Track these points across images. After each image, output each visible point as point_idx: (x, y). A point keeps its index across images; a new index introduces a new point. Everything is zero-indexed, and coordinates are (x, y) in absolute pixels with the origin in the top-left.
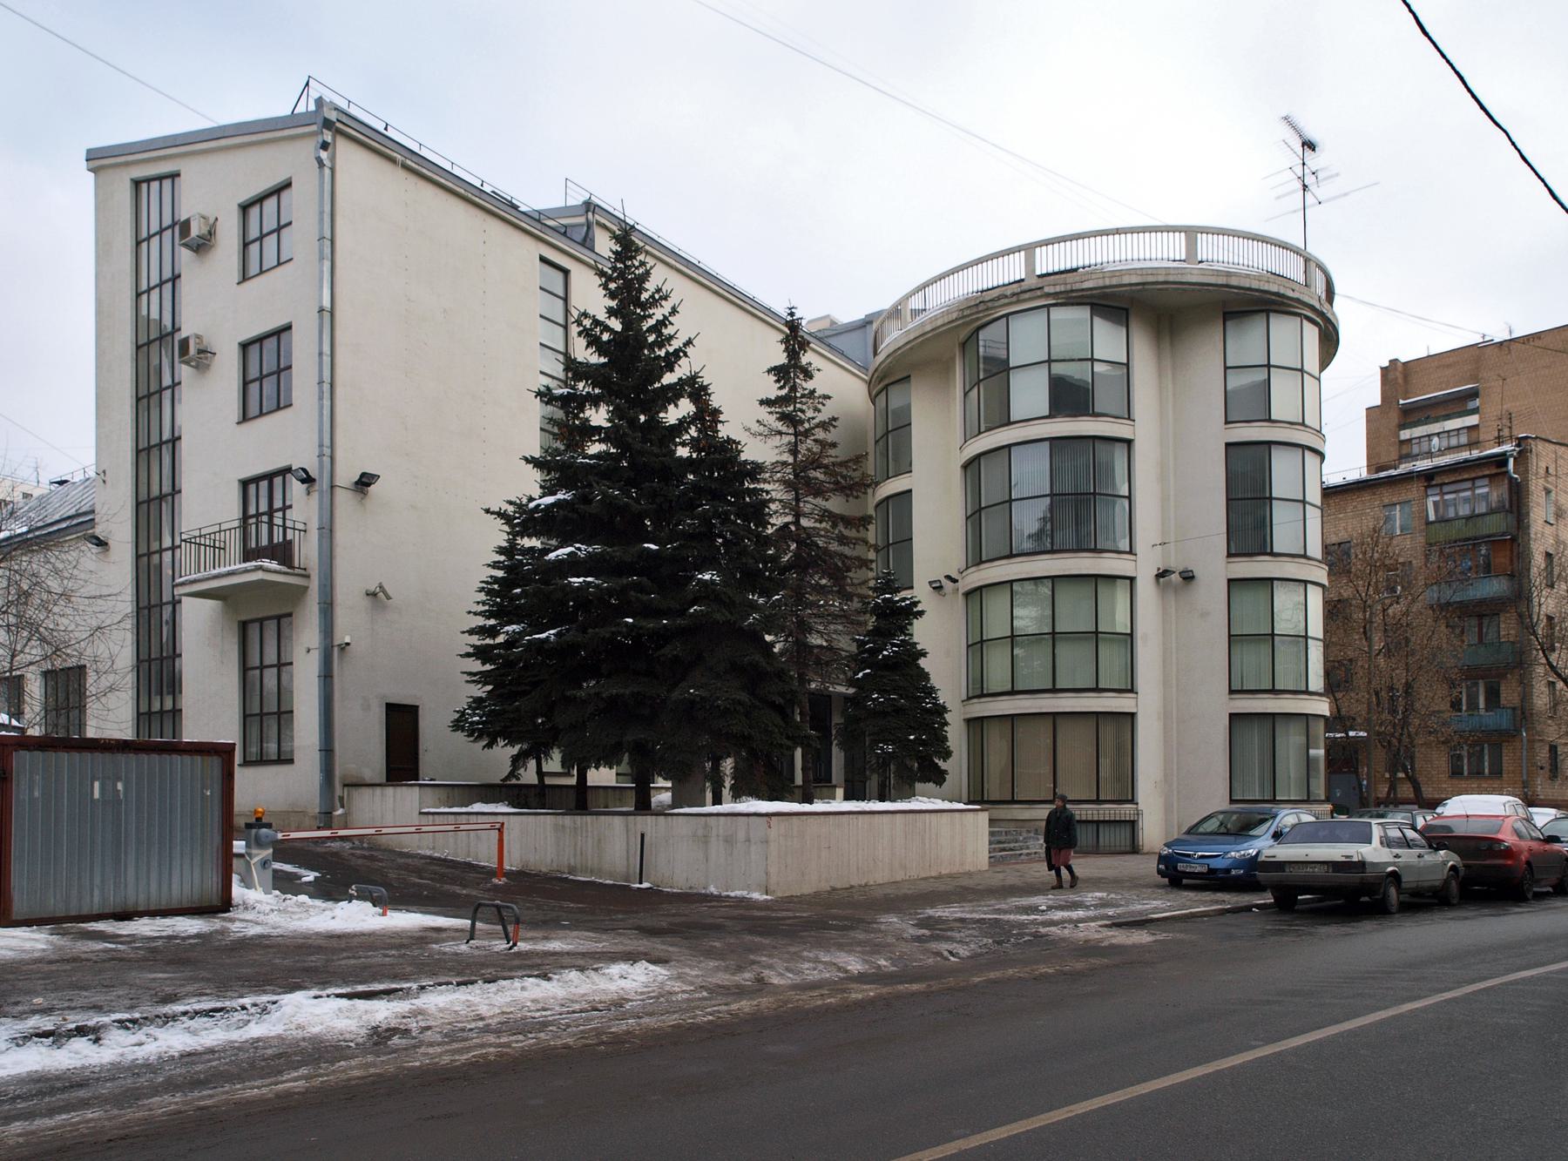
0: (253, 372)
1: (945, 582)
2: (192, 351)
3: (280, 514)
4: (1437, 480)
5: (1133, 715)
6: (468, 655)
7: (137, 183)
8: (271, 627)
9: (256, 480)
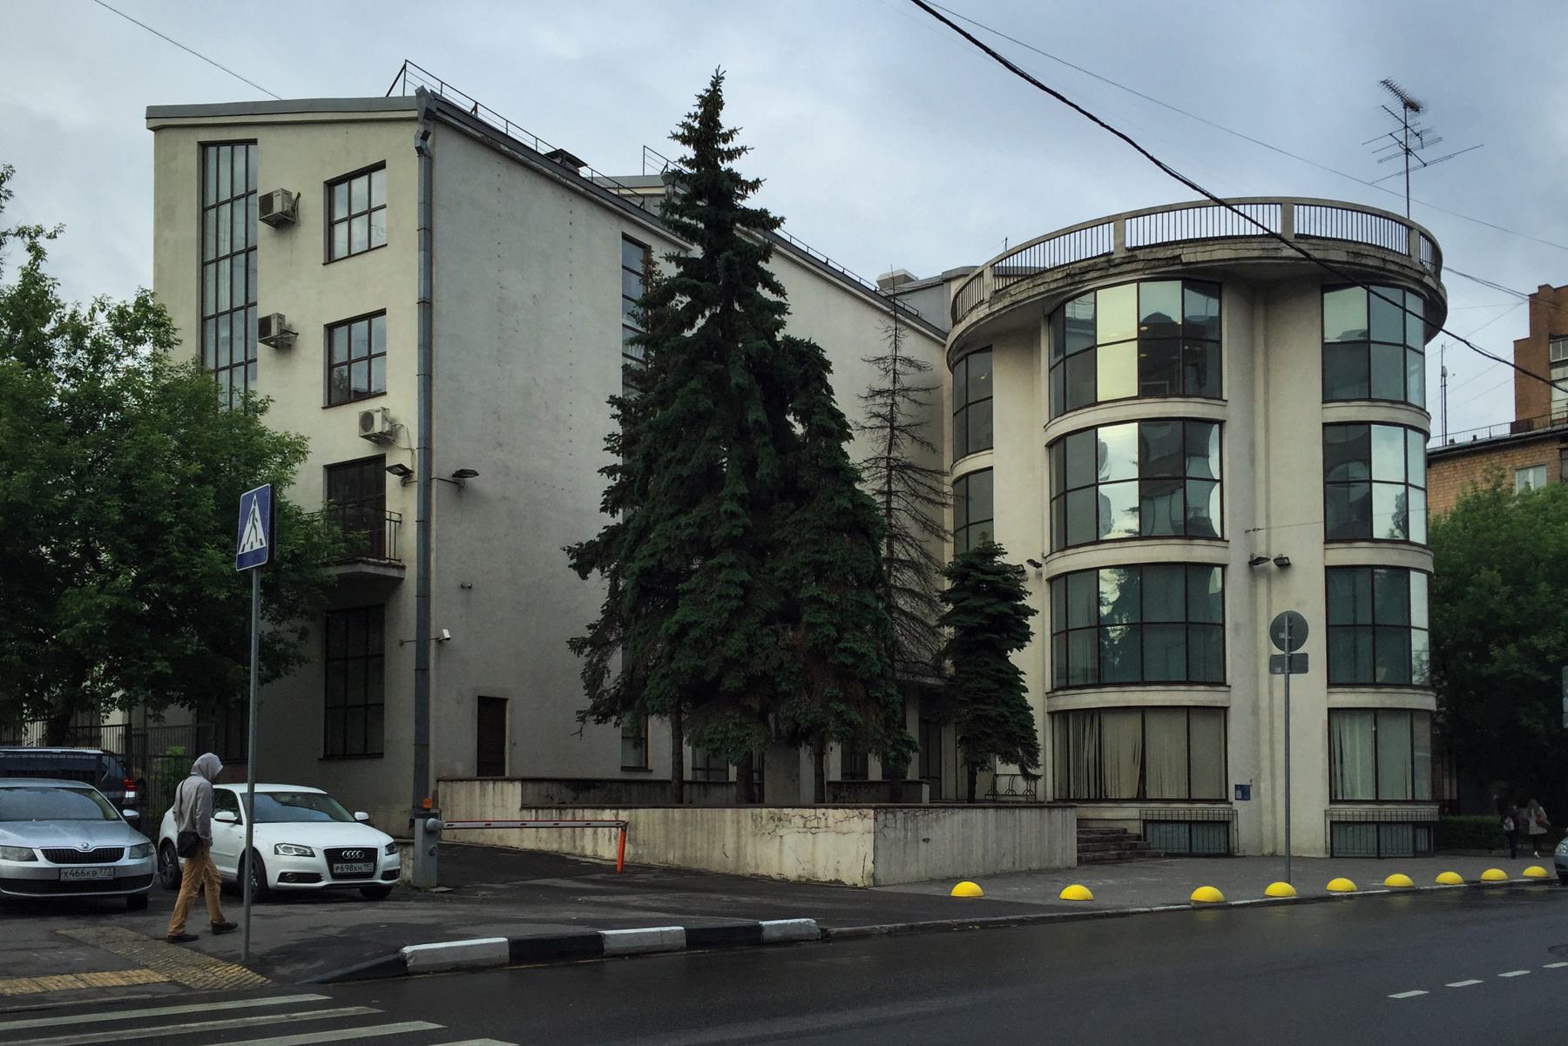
2: (274, 331)
5: (1225, 709)
7: (204, 146)
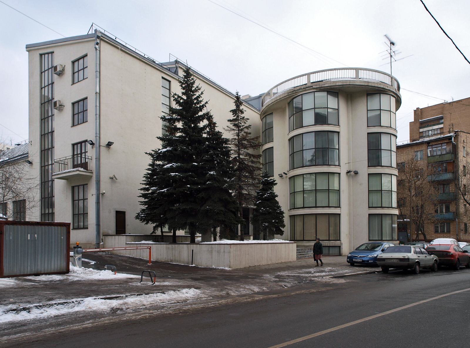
1: (284, 175)
2: (58, 105)
5: (339, 214)
7: (41, 55)
8: (81, 188)
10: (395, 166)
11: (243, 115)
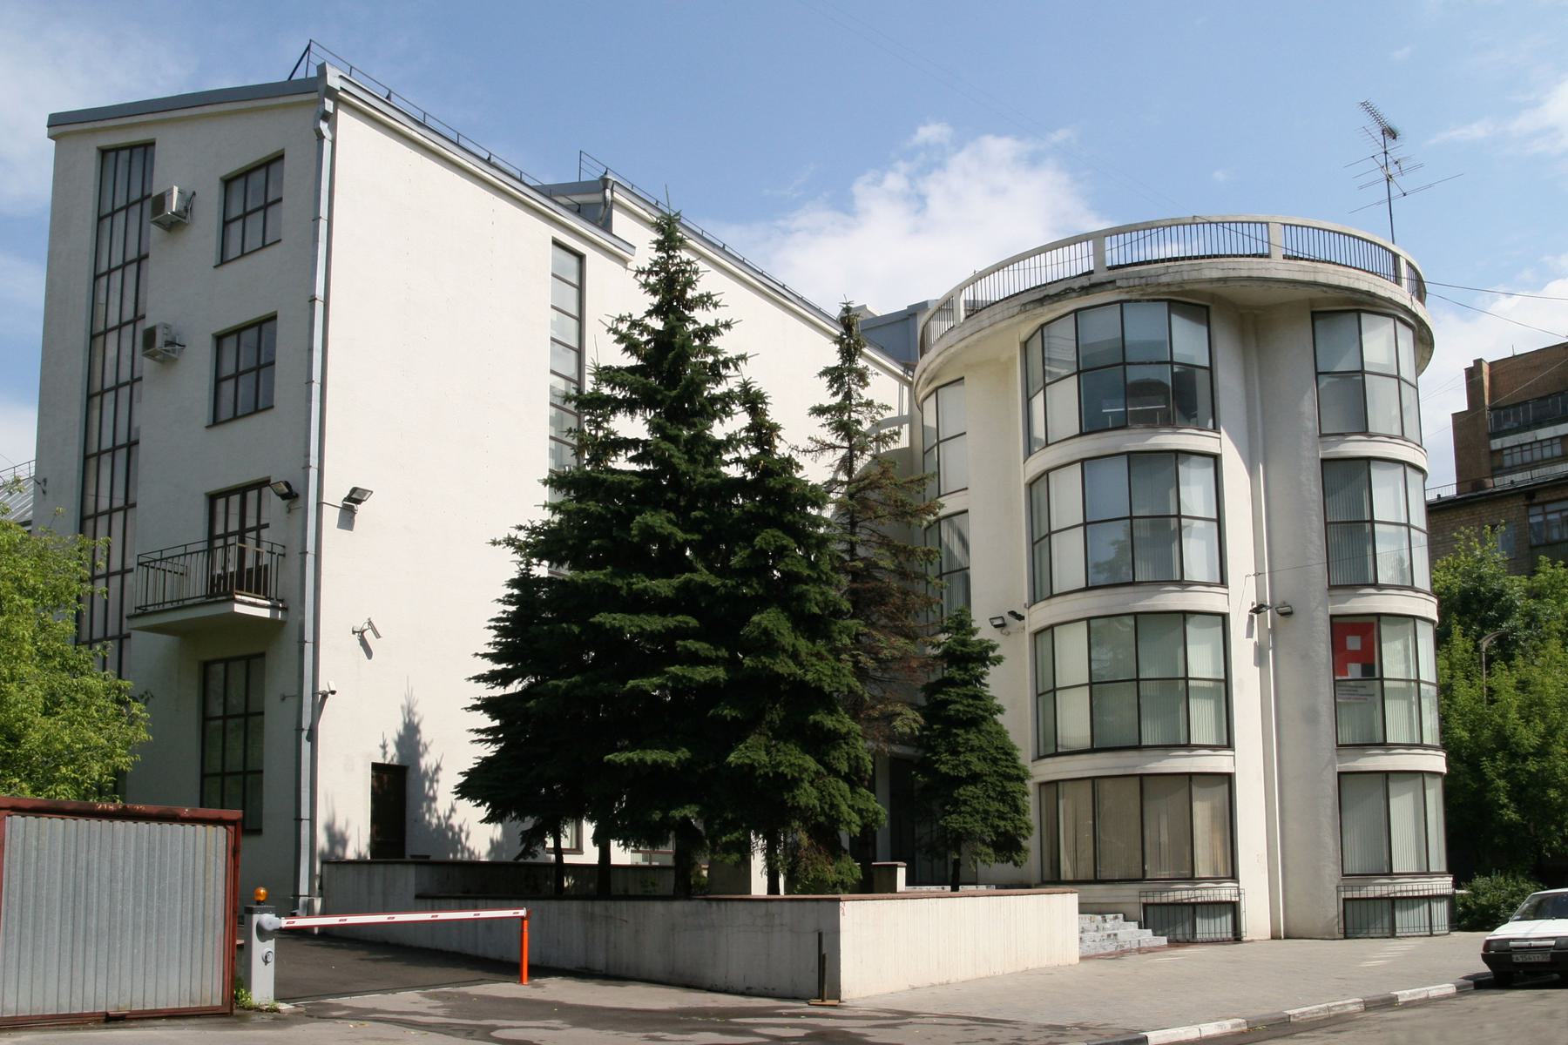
0: (228, 368)
1: (1010, 620)
2: (159, 342)
3: (253, 534)
4: (1539, 498)
6: (475, 708)
7: (104, 152)
8: (238, 671)
9: (226, 494)
10: (1427, 588)
11: (867, 394)
